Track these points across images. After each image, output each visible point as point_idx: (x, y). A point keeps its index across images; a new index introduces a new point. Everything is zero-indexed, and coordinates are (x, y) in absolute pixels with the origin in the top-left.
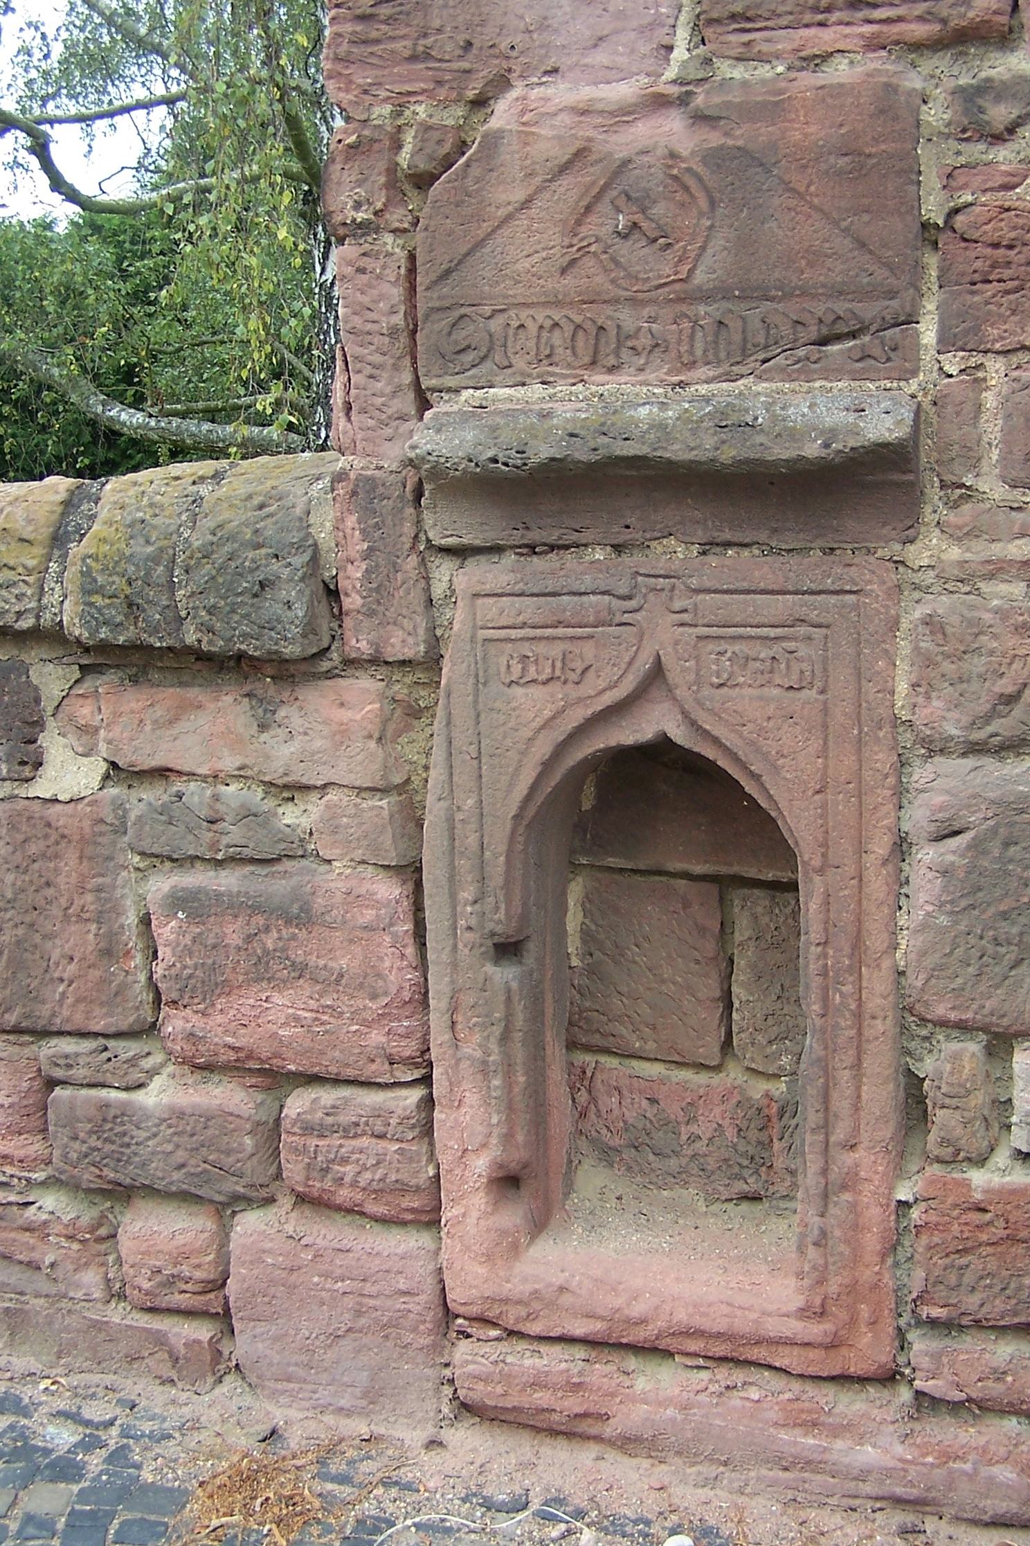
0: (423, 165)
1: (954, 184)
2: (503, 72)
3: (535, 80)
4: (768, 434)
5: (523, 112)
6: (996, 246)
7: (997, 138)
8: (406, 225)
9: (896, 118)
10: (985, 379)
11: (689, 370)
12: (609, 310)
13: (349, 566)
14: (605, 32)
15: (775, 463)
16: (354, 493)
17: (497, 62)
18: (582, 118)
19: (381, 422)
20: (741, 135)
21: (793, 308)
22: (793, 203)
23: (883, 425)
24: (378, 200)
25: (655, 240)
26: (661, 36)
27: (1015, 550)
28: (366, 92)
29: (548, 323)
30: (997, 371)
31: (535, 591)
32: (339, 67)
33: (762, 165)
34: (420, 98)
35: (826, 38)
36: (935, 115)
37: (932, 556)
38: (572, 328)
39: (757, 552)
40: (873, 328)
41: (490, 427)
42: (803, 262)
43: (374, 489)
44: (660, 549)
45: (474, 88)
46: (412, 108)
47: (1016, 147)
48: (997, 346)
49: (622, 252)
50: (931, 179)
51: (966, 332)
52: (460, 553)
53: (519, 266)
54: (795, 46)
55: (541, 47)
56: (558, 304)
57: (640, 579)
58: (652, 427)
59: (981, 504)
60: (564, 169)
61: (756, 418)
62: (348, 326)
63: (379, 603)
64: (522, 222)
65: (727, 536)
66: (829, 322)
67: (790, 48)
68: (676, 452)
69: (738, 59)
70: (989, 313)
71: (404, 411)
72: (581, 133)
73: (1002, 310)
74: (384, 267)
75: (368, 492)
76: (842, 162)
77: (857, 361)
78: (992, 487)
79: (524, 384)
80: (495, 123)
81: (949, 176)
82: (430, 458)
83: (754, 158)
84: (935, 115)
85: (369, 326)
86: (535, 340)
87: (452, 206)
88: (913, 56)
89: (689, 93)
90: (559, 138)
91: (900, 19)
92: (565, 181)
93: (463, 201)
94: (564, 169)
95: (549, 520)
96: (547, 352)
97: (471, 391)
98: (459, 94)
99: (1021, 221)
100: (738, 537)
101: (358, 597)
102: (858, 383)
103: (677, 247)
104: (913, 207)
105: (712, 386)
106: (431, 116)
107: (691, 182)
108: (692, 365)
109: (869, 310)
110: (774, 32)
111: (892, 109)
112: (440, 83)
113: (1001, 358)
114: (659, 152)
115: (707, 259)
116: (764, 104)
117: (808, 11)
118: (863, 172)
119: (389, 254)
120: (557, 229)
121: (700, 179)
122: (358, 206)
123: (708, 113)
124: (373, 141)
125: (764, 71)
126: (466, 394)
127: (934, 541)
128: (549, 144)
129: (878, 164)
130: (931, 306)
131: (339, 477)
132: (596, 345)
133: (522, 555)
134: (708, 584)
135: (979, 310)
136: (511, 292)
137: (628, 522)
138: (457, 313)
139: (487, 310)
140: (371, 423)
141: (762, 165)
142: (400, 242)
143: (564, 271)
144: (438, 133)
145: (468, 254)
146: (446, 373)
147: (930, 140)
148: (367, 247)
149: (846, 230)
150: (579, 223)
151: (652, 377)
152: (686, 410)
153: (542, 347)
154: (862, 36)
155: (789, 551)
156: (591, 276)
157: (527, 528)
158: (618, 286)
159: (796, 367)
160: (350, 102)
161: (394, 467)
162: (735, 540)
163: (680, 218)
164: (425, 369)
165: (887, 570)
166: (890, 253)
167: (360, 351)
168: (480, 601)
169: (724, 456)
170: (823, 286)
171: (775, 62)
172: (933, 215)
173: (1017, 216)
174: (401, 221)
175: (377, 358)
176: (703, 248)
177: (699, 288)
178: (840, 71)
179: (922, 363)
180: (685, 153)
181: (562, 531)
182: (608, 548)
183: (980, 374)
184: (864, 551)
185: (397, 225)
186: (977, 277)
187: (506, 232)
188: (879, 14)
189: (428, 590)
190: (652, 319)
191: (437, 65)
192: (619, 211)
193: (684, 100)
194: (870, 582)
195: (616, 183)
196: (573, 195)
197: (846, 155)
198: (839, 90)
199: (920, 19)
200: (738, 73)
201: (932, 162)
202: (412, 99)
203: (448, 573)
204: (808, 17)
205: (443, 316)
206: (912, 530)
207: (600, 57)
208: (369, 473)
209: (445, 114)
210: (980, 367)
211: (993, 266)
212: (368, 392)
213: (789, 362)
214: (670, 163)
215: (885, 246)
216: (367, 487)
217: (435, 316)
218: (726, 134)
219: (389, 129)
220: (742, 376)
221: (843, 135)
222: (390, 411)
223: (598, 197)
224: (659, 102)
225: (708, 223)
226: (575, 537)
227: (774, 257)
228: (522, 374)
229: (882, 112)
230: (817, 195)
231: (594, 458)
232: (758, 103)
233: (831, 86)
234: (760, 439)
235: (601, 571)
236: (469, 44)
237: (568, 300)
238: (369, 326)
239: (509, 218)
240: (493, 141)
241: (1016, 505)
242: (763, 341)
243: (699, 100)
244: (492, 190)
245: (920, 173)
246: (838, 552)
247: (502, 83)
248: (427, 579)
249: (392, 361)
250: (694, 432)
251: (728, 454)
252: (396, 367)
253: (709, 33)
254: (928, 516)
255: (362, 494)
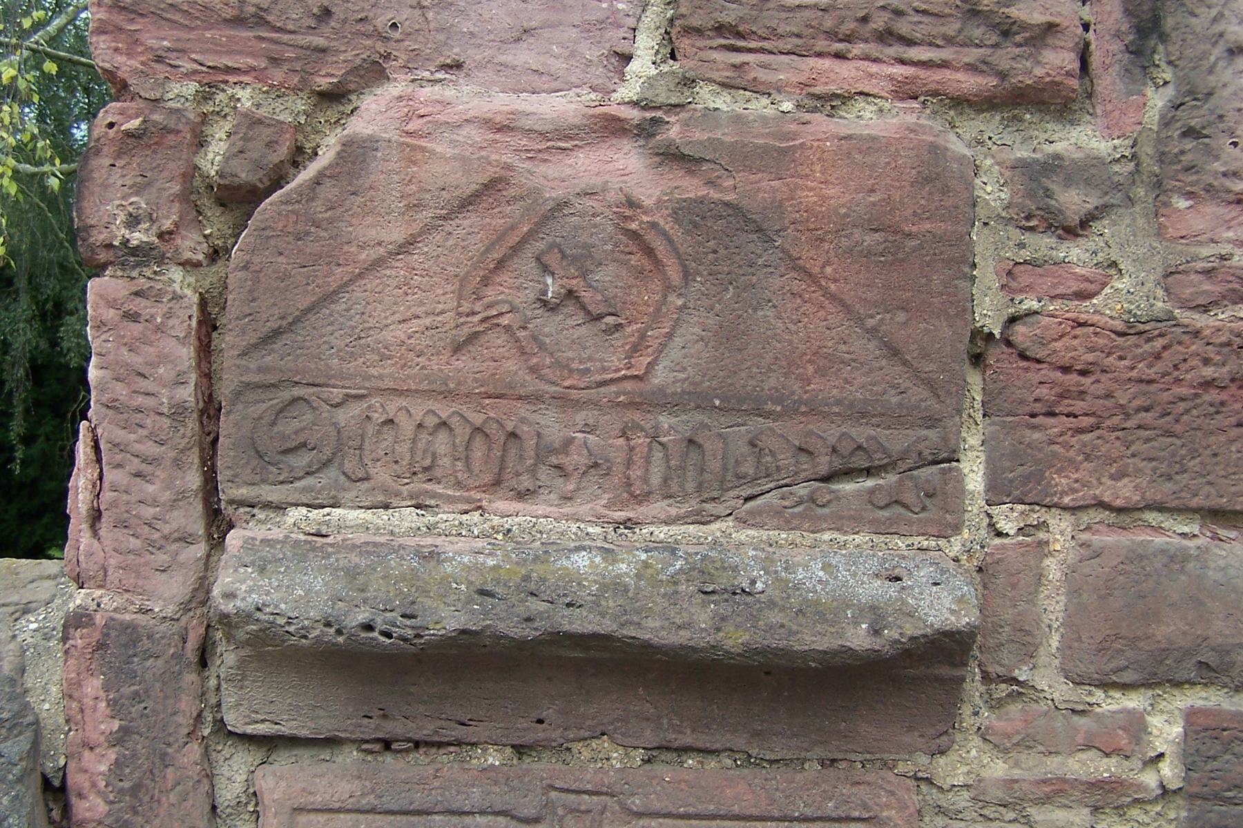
0: (245, 174)
1: (1014, 284)
2: (376, 57)
3: (427, 74)
4: (783, 609)
5: (408, 118)
6: (1066, 370)
7: (1070, 232)
8: (201, 257)
9: (945, 190)
10: (1047, 543)
11: (640, 503)
12: (523, 410)
13: (87, 753)
14: (533, 24)
15: (804, 655)
16: (101, 646)
17: (369, 42)
18: (498, 136)
19: (152, 543)
20: (733, 187)
21: (793, 430)
22: (797, 286)
23: (941, 605)
24: (168, 218)
25: (599, 318)
26: (615, 39)
27: (1077, 766)
28: (159, 59)
29: (431, 421)
30: (1062, 533)
31: (395, 807)
32: (119, 19)
33: (760, 230)
34: (245, 79)
35: (843, 75)
36: (992, 192)
37: (969, 773)
38: (468, 431)
39: (729, 762)
40: (903, 466)
41: (347, 570)
42: (811, 368)
43: (134, 642)
44: (586, 754)
45: (332, 75)
46: (230, 91)
47: (1091, 245)
48: (1067, 500)
49: (547, 330)
50: (987, 275)
51: (1027, 478)
52: (270, 743)
53: (387, 335)
54: (803, 79)
55: (440, 30)
56: (447, 395)
57: (553, 794)
58: (604, 588)
59: (1034, 706)
60: (466, 204)
61: (753, 582)
62: (105, 398)
63: (136, 813)
64: (397, 271)
65: (688, 739)
66: (846, 453)
67: (795, 80)
68: (654, 629)
69: (723, 85)
70: (1055, 455)
71: (190, 529)
72: (494, 157)
73: (1072, 453)
74: (168, 315)
75: (125, 646)
76: (870, 239)
77: (881, 508)
78: (1050, 682)
79: (386, 507)
80: (358, 126)
81: (1009, 273)
82: (258, 615)
83: (748, 221)
84: (992, 192)
85: (140, 400)
86: (409, 444)
87: (291, 238)
88: (952, 113)
89: (654, 121)
90: (463, 160)
91: (945, 65)
92: (468, 221)
93: (308, 234)
94: (466, 204)
95: (422, 708)
96: (427, 462)
97: (304, 510)
98: (303, 80)
99: (1101, 341)
100: (703, 741)
101: (99, 801)
102: (882, 538)
103: (629, 330)
104: (964, 310)
105: (674, 529)
106: (258, 106)
107: (659, 245)
108: (643, 498)
109: (898, 440)
110: (772, 57)
111: (938, 178)
112: (275, 61)
113: (1067, 516)
114: (612, 196)
115: (675, 352)
116: (766, 149)
117: (823, 36)
118: (900, 256)
119: (176, 297)
120: (449, 288)
121: (670, 241)
122: (133, 221)
123: (686, 151)
124: (166, 130)
125: (760, 106)
126: (295, 514)
127: (974, 753)
128: (448, 165)
129: (921, 247)
130: (974, 440)
131: (78, 620)
132: (503, 459)
133: (371, 752)
134: (657, 806)
135: (1040, 450)
136: (373, 371)
137: (543, 715)
138: (286, 395)
139: (337, 394)
140: (134, 543)
141: (760, 230)
142: (192, 280)
143: (457, 349)
144: (269, 131)
145: (309, 310)
146: (263, 481)
147: (986, 224)
148: (142, 283)
149: (873, 331)
150: (485, 282)
151: (584, 509)
152: (646, 565)
153: (419, 454)
154: (891, 78)
155: (771, 762)
156: (498, 359)
157: (385, 716)
158: (541, 378)
159: (796, 510)
160: (134, 71)
161: (170, 611)
162: (700, 745)
163: (634, 290)
164: (229, 473)
165: (908, 790)
166: (932, 367)
167: (120, 435)
168: (303, 819)
169: (731, 642)
170: (839, 402)
171: (775, 96)
172: (988, 321)
173: (1096, 334)
174: (194, 250)
175: (150, 449)
176: (670, 336)
177: (661, 390)
178: (864, 119)
179: (967, 516)
180: (648, 203)
181: (439, 723)
182: (509, 750)
183: (1042, 535)
184: (878, 764)
185: (188, 255)
186: (1038, 407)
187: (371, 283)
188: (915, 53)
189: (211, 794)
190: (589, 429)
191: (274, 35)
192: (546, 269)
193: (646, 130)
194: (888, 806)
195: (541, 235)
196: (477, 244)
197: (876, 230)
198: (870, 145)
199: (971, 68)
200: (723, 102)
201: (990, 250)
202: (232, 79)
203: (244, 769)
204: (822, 44)
205: (263, 396)
206: (944, 738)
207: (523, 56)
208: (128, 617)
209: (278, 106)
210: (1043, 525)
211: (1062, 396)
212: (133, 498)
213: (786, 503)
214: (628, 213)
215: (925, 356)
216: (124, 639)
217: (252, 396)
218: (710, 183)
219: (192, 116)
220: (719, 517)
221: (874, 204)
222: (167, 529)
223: (516, 250)
224: (612, 128)
225: (680, 302)
226: (459, 732)
227: (769, 358)
228: (385, 491)
229: (928, 180)
230: (835, 281)
231: (529, 633)
232: (757, 147)
233: (861, 138)
234: (775, 617)
235: (496, 783)
236: (327, 13)
237: (464, 390)
238: (140, 400)
239: (378, 263)
240: (356, 154)
241: (1080, 707)
242: (751, 472)
243: (673, 132)
244: (354, 221)
245: (974, 266)
246: (842, 765)
247: (375, 72)
248: (210, 777)
249: (172, 454)
250: (672, 598)
251: (736, 638)
252: (178, 464)
253: (684, 44)
254: (968, 721)
255: (114, 648)
